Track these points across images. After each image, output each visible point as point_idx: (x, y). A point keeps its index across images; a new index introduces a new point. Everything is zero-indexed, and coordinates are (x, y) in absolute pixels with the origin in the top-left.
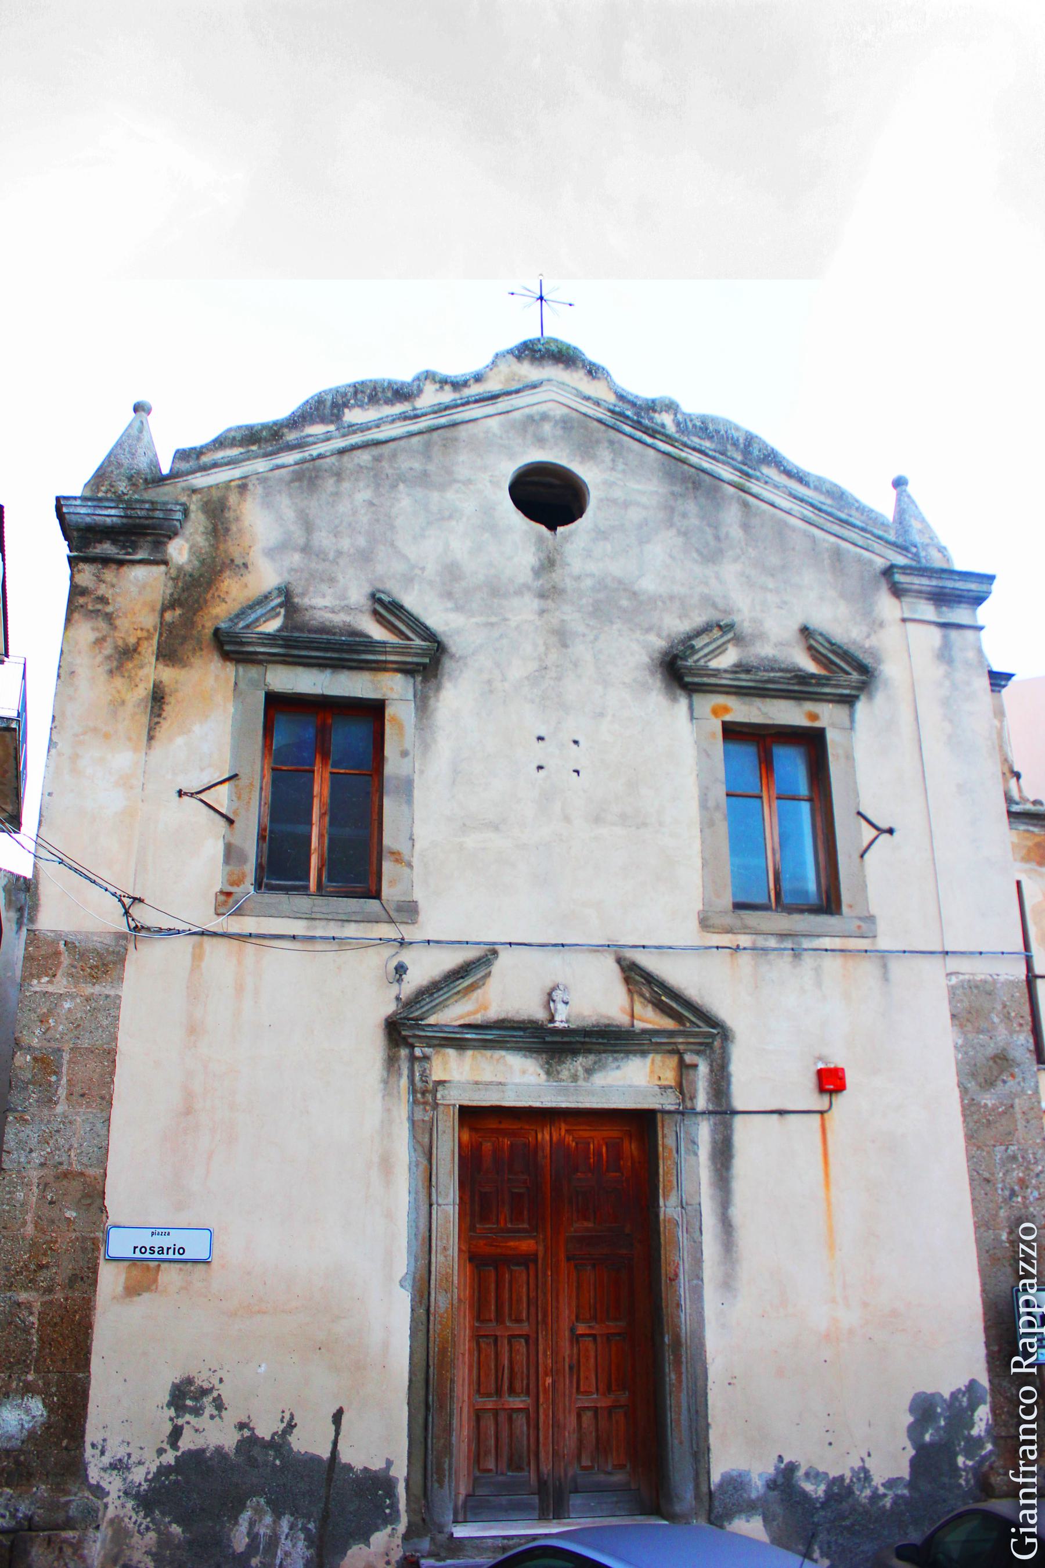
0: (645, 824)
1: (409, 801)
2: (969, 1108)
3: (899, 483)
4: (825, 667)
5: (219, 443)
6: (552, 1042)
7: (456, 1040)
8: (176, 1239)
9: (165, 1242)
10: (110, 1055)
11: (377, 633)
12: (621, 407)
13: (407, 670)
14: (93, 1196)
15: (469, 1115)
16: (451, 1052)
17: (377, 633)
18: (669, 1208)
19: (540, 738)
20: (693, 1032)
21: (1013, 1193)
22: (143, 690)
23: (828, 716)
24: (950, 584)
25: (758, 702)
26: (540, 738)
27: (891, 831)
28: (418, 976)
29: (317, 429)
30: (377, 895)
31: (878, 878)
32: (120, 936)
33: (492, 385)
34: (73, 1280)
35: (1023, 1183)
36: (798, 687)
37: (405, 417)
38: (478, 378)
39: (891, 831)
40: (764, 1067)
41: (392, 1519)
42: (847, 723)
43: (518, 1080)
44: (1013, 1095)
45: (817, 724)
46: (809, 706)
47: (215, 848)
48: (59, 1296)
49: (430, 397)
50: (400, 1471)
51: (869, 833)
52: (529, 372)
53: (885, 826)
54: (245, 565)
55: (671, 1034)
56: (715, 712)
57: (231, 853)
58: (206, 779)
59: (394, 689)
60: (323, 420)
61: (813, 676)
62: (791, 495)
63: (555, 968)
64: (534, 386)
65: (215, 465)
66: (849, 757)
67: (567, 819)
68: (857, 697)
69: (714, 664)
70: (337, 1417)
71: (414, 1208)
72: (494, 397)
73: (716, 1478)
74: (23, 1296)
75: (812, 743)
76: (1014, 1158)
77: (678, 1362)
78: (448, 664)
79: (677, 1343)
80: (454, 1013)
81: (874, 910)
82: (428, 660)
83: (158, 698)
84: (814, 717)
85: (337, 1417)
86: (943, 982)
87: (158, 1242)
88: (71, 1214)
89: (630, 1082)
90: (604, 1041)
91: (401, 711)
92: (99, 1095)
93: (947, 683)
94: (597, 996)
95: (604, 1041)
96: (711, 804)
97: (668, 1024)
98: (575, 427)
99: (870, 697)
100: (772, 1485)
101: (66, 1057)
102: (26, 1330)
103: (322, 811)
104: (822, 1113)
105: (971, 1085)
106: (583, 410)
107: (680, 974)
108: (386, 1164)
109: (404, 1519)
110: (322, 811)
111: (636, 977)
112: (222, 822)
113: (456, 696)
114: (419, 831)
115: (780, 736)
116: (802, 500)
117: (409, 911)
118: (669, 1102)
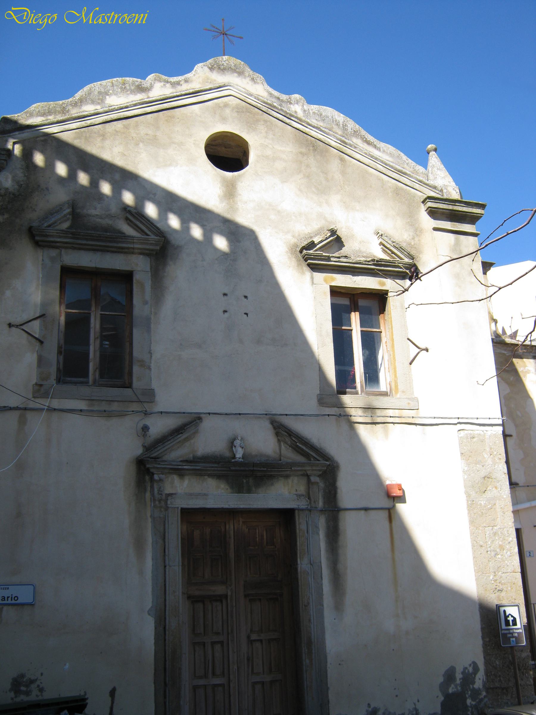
2: (471, 505)
8: (13, 591)
18: (303, 564)
19: (225, 295)
30: (130, 386)
35: (502, 547)
43: (216, 494)
53: (423, 347)
55: (302, 465)
57: (41, 361)
60: (93, 102)
75: (380, 299)
76: (495, 534)
79: (310, 643)
80: (176, 453)
85: (112, 693)
89: (280, 495)
94: (262, 442)
105: (473, 493)
111: (281, 430)
112: (38, 344)
117: (150, 395)
118: (303, 504)
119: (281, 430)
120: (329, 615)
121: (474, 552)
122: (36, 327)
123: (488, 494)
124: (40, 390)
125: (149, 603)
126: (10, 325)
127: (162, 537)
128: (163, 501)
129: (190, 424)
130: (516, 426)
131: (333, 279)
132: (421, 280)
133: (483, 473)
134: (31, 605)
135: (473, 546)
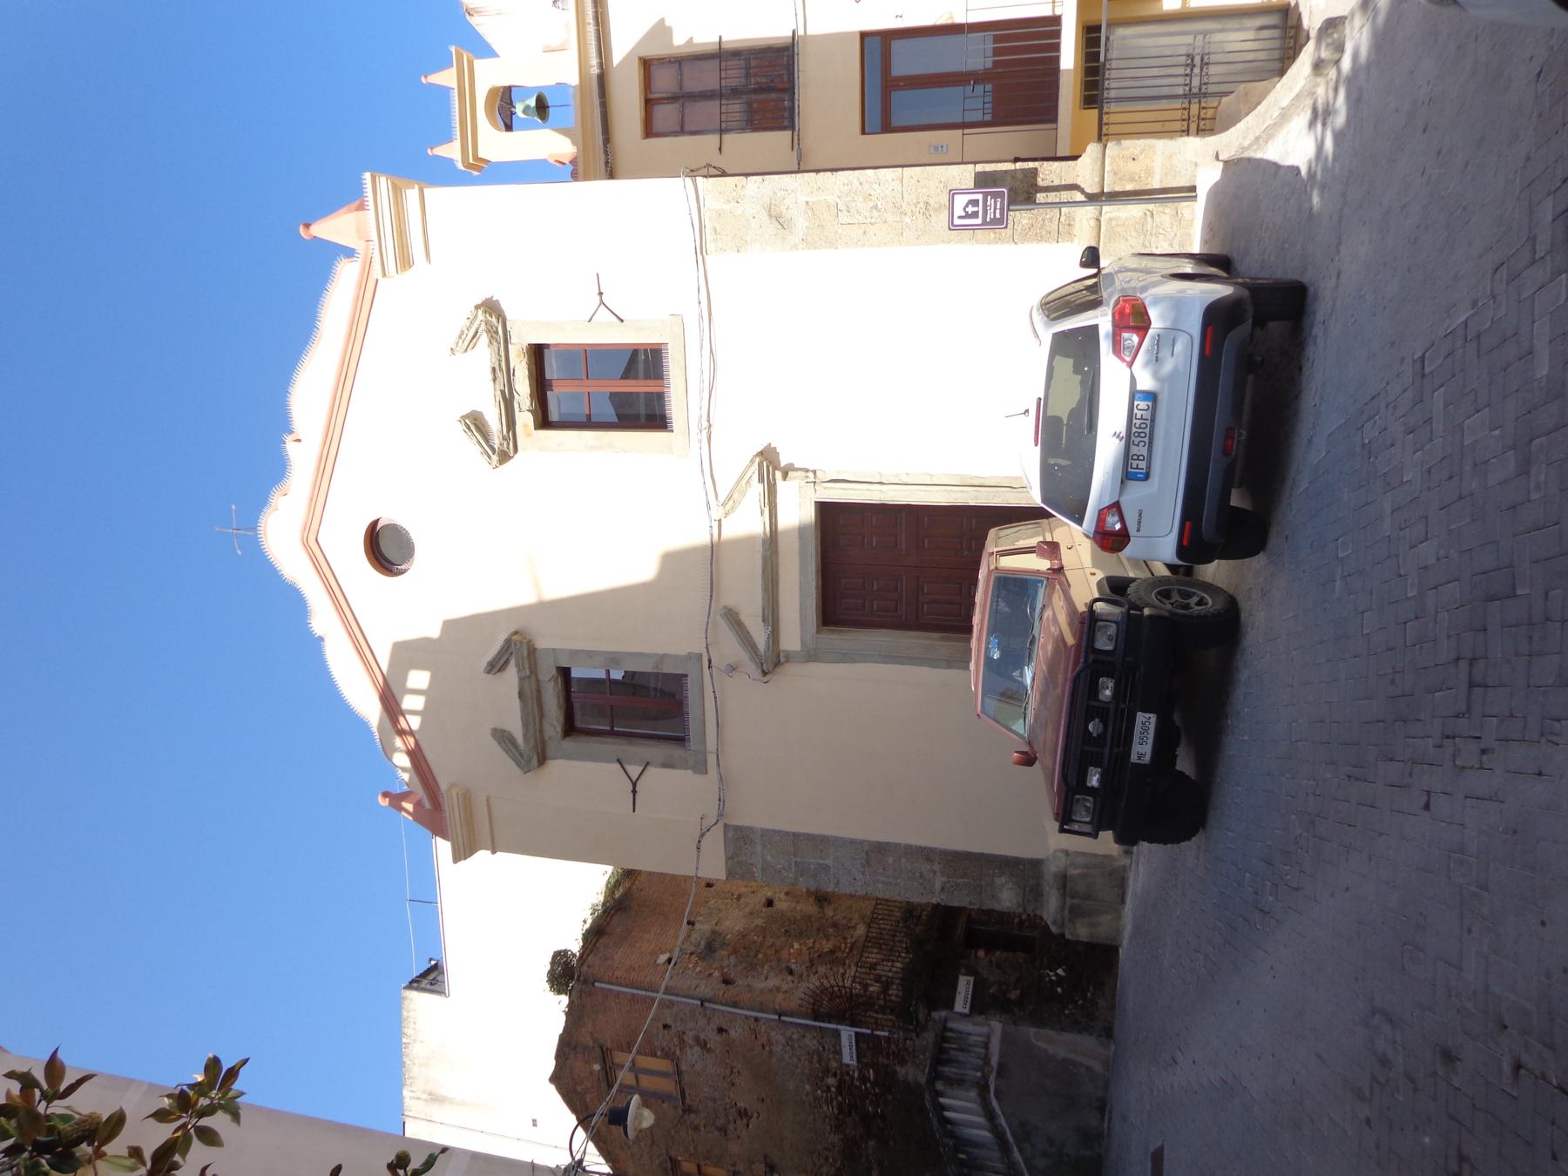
7: (774, 636)
21: (876, 207)
74: (938, 886)
80: (760, 636)
88: (891, 860)
122: (634, 770)
124: (701, 767)
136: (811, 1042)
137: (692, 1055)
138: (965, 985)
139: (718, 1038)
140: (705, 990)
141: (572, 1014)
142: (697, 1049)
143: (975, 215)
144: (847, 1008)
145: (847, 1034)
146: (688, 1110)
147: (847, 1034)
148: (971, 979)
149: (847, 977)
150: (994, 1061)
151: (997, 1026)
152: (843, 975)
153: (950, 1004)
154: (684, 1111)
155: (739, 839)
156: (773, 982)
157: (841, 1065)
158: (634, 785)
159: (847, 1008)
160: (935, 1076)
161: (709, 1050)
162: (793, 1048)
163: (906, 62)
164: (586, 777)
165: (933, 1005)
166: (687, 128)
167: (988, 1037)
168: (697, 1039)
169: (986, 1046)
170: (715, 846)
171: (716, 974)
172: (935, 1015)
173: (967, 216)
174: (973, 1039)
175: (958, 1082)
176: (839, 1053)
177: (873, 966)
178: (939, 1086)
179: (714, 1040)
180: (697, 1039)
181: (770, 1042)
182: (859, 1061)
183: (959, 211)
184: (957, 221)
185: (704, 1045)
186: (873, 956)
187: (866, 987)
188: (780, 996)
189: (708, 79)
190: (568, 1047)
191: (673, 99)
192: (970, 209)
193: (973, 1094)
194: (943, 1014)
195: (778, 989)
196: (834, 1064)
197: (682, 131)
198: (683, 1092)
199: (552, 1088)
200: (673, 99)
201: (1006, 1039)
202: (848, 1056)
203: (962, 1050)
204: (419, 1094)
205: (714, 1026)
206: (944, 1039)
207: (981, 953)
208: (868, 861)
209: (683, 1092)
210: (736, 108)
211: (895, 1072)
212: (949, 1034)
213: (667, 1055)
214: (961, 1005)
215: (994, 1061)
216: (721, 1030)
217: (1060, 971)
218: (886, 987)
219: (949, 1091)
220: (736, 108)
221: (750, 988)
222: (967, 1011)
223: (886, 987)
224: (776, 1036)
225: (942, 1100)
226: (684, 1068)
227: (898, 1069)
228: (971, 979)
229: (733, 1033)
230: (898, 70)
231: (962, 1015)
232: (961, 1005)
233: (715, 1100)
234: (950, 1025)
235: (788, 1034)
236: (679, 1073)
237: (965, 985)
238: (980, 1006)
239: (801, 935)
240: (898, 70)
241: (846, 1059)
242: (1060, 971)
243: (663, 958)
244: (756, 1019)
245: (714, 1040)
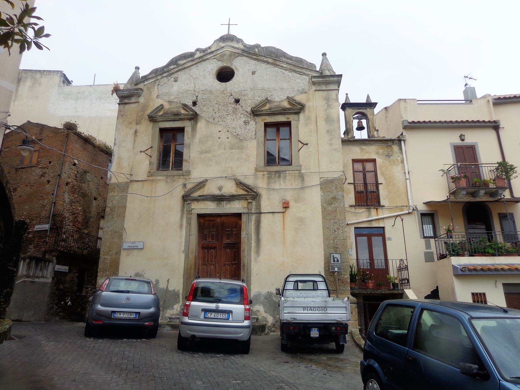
0: (243, 148)
1: (189, 148)
2: (324, 209)
3: (324, 55)
4: (292, 106)
5: (150, 73)
6: (219, 199)
7: (196, 200)
8: (137, 244)
9: (134, 245)
10: (125, 207)
11: (183, 112)
12: (245, 48)
13: (190, 119)
14: (120, 237)
15: (200, 216)
16: (196, 202)
17: (183, 112)
18: (243, 235)
19: (220, 131)
20: (251, 194)
21: (335, 231)
22: (133, 131)
23: (292, 118)
24: (327, 79)
25: (274, 117)
26: (220, 131)
27: (307, 144)
28: (189, 186)
29: (172, 67)
30: (182, 170)
31: (304, 158)
32: (127, 183)
33: (213, 49)
34: (117, 253)
35: (338, 229)
36: (284, 112)
37: (192, 61)
38: (209, 48)
39: (307, 144)
40: (269, 202)
41: (179, 302)
42: (297, 119)
43: (210, 208)
44: (336, 207)
45: (289, 120)
46: (287, 116)
47: (147, 162)
48: (113, 257)
49: (198, 55)
50: (181, 292)
51: (301, 145)
52: (222, 44)
53: (305, 143)
54: (173, 181)
55: (245, 195)
56: (262, 120)
57: (151, 163)
58: (146, 148)
59: (187, 125)
60: (173, 65)
61: (288, 108)
62: (287, 63)
63: (221, 182)
64: (223, 48)
65: (149, 79)
66: (297, 127)
67: (225, 149)
68: (300, 112)
69: (263, 109)
70: (168, 281)
71: (186, 236)
72: (212, 52)
73: (252, 295)
74: (107, 257)
75: (288, 124)
76: (336, 223)
77: (244, 269)
78: (199, 117)
79: (244, 265)
80: (196, 194)
81: (301, 163)
82: (194, 117)
83: (136, 132)
84: (288, 118)
85: (168, 281)
86: (319, 180)
87: (133, 245)
88: (116, 240)
89: (236, 207)
90: (232, 198)
91: (188, 130)
92: (122, 216)
93: (326, 105)
94: (230, 189)
95: (232, 198)
96: (260, 142)
97: (245, 193)
98: (234, 55)
99: (304, 112)
100: (266, 298)
101: (116, 208)
102: (107, 264)
103: (170, 151)
104: (283, 212)
105: (325, 205)
106: (234, 51)
107: (249, 182)
108: (181, 226)
109: (181, 302)
110: (170, 151)
111: (240, 184)
112: (149, 157)
113: (201, 125)
114: (191, 155)
115: (278, 122)
116: (290, 64)
117: (189, 173)
118: (245, 211)
119: (240, 184)
120: (253, 254)
121: (323, 230)
122: (149, 152)
123: (333, 205)
124: (150, 174)
125: (183, 248)
126: (141, 152)
127: (189, 224)
128: (190, 212)
129: (202, 184)
130: (385, 179)
131: (265, 119)
132: (368, 97)
133: (332, 196)
134: (142, 249)
135: (323, 228)
136: (44, 213)
137: (39, 171)
138: (65, 268)
139: (45, 181)
140: (64, 176)
141: (55, 130)
142: (41, 173)
143: (334, 261)
144: (57, 227)
145: (47, 227)
146: (17, 170)
147: (47, 227)
148: (67, 271)
149: (69, 226)
150: (36, 280)
151: (50, 280)
152: (69, 225)
153: (58, 263)
154: (16, 169)
155: (124, 187)
156: (67, 200)
157: (35, 225)
158: (304, 144)
159: (57, 227)
160: (31, 258)
161: (40, 178)
162: (41, 207)
163: (377, 241)
164: (148, 137)
165: (57, 258)
166: (355, 173)
167: (46, 278)
168: (45, 173)
169: (43, 277)
170: (122, 179)
171: (70, 180)
172: (54, 258)
173: (334, 258)
174: (45, 272)
175: (29, 268)
176: (40, 223)
177: (72, 236)
178: (28, 260)
179: (44, 180)
180: (45, 173)
181: (44, 199)
182: (36, 231)
183: (335, 256)
184: (332, 255)
185: (42, 176)
186: (76, 236)
187: (64, 233)
188: (62, 203)
189: (370, 178)
190: (42, 127)
191: (364, 169)
192: (336, 259)
193: (25, 273)
194: (55, 261)
195: (64, 202)
196: (34, 222)
197: (354, 172)
198: (24, 168)
199: (25, 121)
200: (364, 169)
201: (45, 284)
202: (38, 227)
203: (41, 268)
204: (20, 74)
205: (50, 179)
206: (45, 262)
207: (77, 274)
208: (116, 232)
209: (24, 168)
210: (361, 188)
211: (31, 244)
212: (47, 263)
213: (38, 163)
214: (58, 268)
215: (36, 280)
216: (49, 182)
217: (70, 303)
218: (64, 240)
219: (26, 264)
220: (361, 188)
221: (64, 192)
222: (56, 269)
223: (64, 240)
224: (46, 201)
225: (22, 261)
226: (33, 168)
227: (33, 245)
228: (67, 271)
229: (48, 186)
230: (374, 238)
231: (54, 268)
232: (58, 268)
233: (21, 179)
234: (51, 264)
235: (47, 206)
236: (32, 167)
237: (65, 268)
238: (57, 274)
239: (84, 211)
240: (374, 238)
241: (36, 227)
242: (70, 303)
243: (76, 162)
244: (53, 194)
245: (44, 180)
